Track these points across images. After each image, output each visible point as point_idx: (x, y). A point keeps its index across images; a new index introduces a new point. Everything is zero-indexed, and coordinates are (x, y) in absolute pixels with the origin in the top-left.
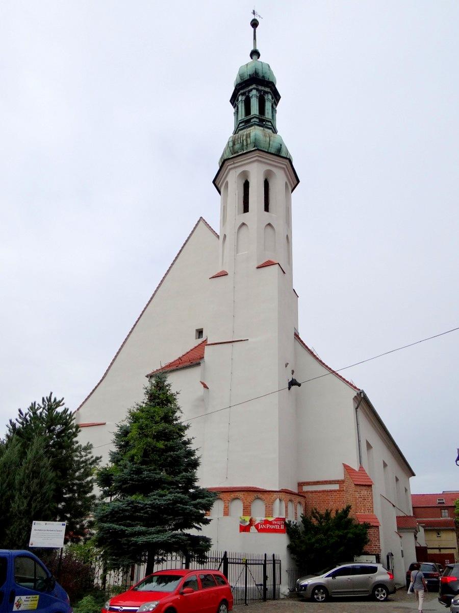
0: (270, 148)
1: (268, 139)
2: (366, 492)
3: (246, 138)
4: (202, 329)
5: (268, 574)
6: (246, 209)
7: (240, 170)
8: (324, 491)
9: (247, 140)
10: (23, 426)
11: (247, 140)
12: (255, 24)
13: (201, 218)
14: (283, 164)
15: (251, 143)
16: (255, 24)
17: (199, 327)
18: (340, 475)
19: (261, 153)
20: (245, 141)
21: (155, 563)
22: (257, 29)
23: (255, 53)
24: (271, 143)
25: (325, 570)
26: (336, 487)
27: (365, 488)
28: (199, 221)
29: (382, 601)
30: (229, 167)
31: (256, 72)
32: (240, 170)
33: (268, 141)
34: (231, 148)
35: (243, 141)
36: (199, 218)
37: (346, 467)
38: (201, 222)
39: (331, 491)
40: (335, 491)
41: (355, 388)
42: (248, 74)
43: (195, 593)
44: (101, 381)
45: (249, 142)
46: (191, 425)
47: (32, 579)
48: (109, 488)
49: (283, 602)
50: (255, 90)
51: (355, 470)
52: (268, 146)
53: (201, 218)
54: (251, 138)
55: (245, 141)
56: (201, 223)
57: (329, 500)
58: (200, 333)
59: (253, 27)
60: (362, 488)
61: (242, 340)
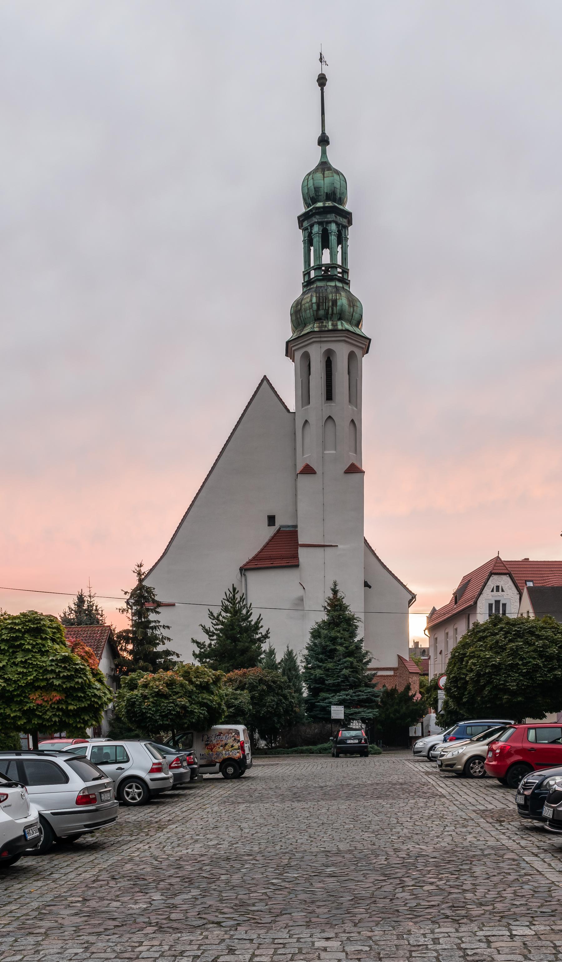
3: (333, 305)
6: (329, 396)
7: (326, 347)
9: (333, 309)
10: (153, 594)
11: (333, 309)
12: (322, 80)
13: (265, 376)
16: (322, 80)
19: (349, 333)
20: (330, 308)
24: (354, 313)
26: (391, 673)
27: (415, 675)
28: (260, 385)
29: (135, 805)
31: (334, 192)
32: (326, 347)
34: (315, 313)
35: (328, 308)
37: (400, 658)
38: (265, 382)
39: (387, 676)
40: (390, 676)
45: (335, 312)
46: (137, 564)
48: (133, 635)
49: (218, 761)
52: (351, 318)
55: (330, 308)
58: (271, 520)
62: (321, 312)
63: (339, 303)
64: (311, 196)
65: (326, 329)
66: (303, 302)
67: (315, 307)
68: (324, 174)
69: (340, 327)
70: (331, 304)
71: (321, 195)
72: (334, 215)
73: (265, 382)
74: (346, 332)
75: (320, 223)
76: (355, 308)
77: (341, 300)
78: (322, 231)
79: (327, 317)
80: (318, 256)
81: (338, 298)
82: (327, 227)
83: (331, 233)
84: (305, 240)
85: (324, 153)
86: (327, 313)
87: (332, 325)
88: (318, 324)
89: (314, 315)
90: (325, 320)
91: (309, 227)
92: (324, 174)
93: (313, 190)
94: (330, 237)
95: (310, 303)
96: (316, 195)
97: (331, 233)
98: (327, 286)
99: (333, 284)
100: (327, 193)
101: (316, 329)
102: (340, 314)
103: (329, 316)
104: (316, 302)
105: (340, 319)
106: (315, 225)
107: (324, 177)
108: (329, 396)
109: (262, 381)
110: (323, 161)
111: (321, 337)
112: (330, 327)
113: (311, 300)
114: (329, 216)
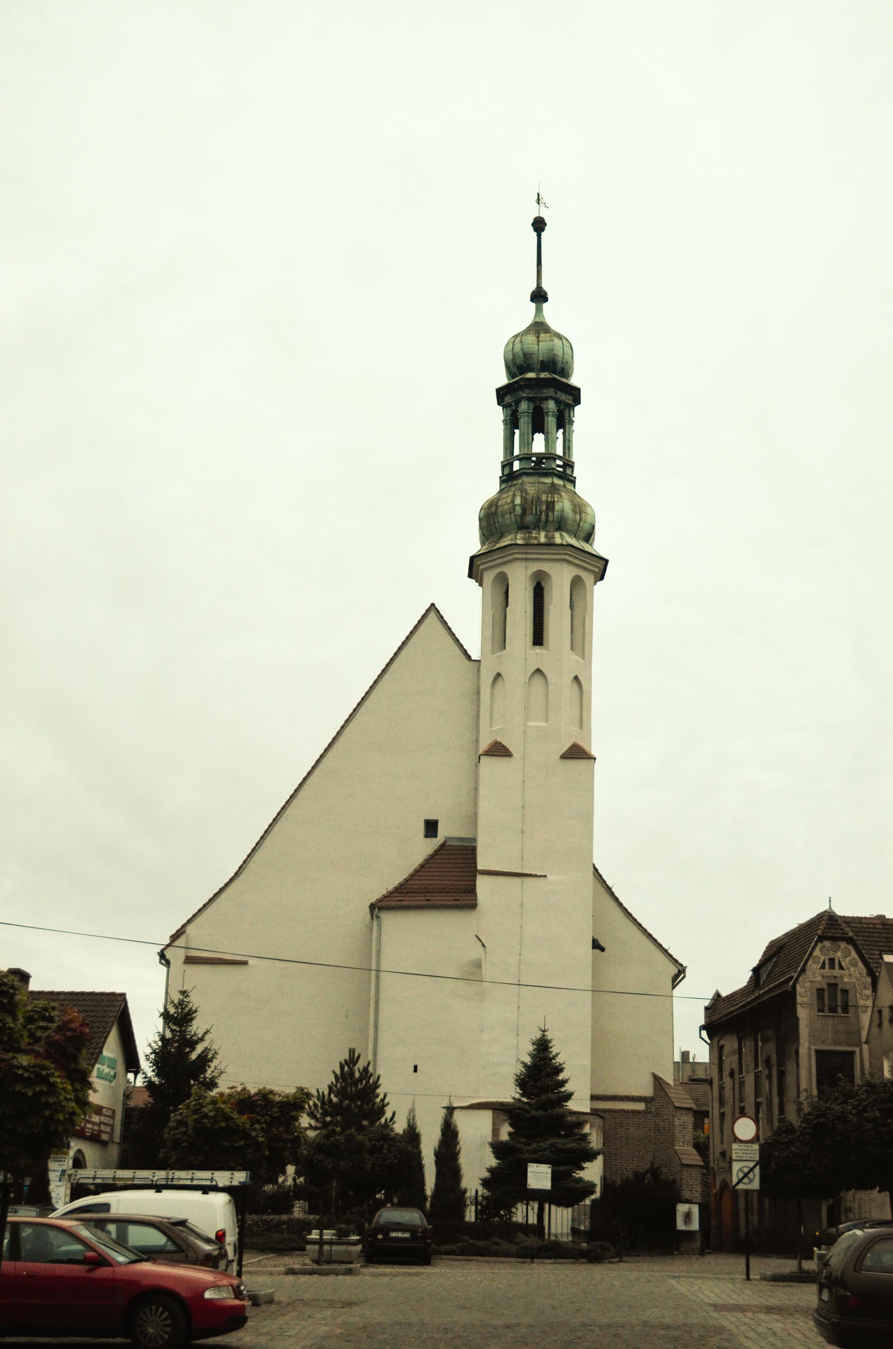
0: (579, 532)
1: (578, 517)
2: (686, 1118)
3: (548, 508)
4: (717, 991)
5: (564, 1220)
6: (538, 639)
7: (534, 567)
8: (623, 1111)
9: (547, 515)
11: (547, 515)
12: (539, 225)
13: (433, 605)
14: (595, 566)
15: (553, 521)
16: (539, 225)
17: (431, 817)
18: (646, 1089)
21: (597, 1195)
22: (534, 287)
23: (539, 296)
25: (237, 1247)
26: (641, 1106)
27: (684, 1112)
28: (424, 617)
30: (481, 567)
32: (534, 567)
33: (578, 521)
34: (519, 519)
35: (541, 512)
36: (429, 605)
38: (432, 614)
40: (639, 1112)
41: (676, 961)
42: (541, 359)
43: (257, 1260)
44: (232, 880)
45: (551, 518)
47: (539, 1207)
50: (553, 402)
51: (669, 1085)
52: (576, 528)
53: (433, 605)
54: (556, 513)
56: (432, 615)
57: (629, 1124)
59: (535, 230)
60: (682, 1112)
61: (536, 876)
62: (529, 518)
63: (558, 507)
64: (518, 364)
65: (536, 542)
66: (500, 503)
67: (518, 510)
68: (538, 337)
69: (558, 540)
70: (544, 507)
71: (534, 364)
72: (552, 389)
73: (432, 614)
74: (571, 548)
75: (530, 399)
76: (583, 515)
77: (560, 504)
78: (534, 409)
79: (537, 526)
80: (526, 442)
81: (556, 499)
82: (542, 405)
83: (547, 413)
84: (507, 420)
85: (539, 310)
86: (539, 520)
87: (546, 537)
88: (523, 535)
89: (516, 522)
90: (534, 529)
91: (513, 404)
92: (538, 337)
93: (522, 356)
94: (546, 418)
95: (511, 505)
96: (526, 363)
97: (547, 413)
98: (539, 482)
99: (548, 480)
100: (542, 362)
101: (520, 542)
102: (559, 523)
103: (542, 524)
104: (521, 505)
105: (559, 528)
106: (523, 402)
107: (538, 341)
108: (538, 639)
109: (428, 611)
110: (537, 320)
111: (526, 553)
112: (543, 540)
113: (513, 501)
114: (545, 391)
